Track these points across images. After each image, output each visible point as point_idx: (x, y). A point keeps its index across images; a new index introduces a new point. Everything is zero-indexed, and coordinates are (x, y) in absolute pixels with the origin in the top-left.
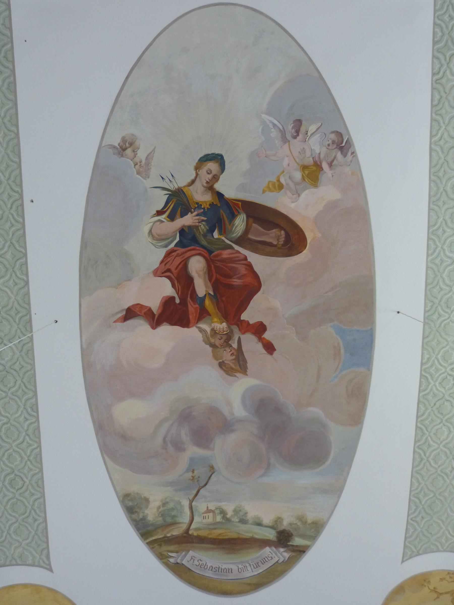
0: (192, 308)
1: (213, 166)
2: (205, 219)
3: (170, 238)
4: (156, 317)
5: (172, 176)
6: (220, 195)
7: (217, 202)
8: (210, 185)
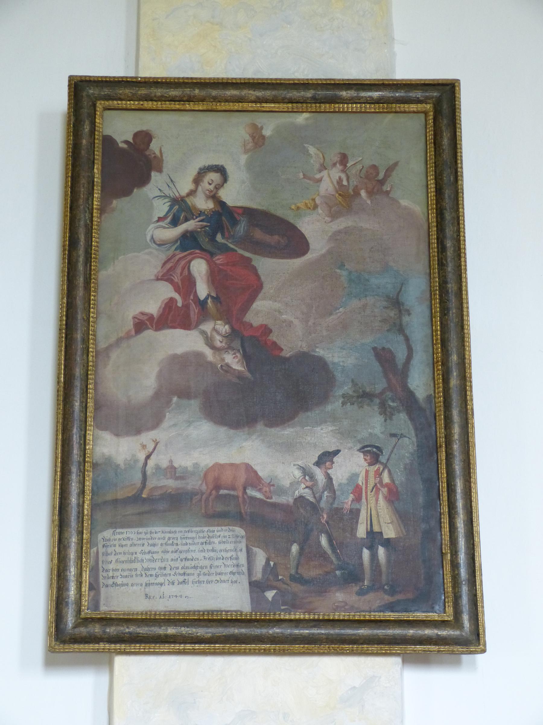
0: (194, 310)
1: (214, 177)
2: (209, 224)
3: (168, 244)
4: (155, 321)
5: (172, 181)
6: (222, 204)
7: (219, 209)
8: (212, 194)
